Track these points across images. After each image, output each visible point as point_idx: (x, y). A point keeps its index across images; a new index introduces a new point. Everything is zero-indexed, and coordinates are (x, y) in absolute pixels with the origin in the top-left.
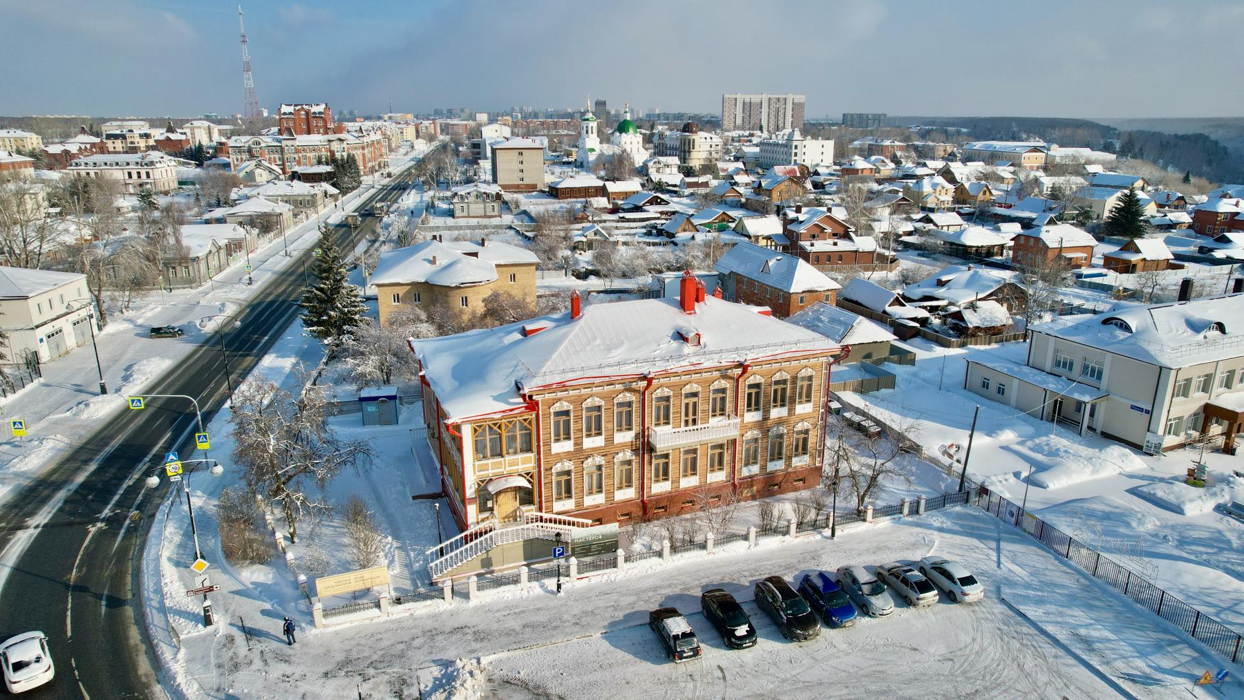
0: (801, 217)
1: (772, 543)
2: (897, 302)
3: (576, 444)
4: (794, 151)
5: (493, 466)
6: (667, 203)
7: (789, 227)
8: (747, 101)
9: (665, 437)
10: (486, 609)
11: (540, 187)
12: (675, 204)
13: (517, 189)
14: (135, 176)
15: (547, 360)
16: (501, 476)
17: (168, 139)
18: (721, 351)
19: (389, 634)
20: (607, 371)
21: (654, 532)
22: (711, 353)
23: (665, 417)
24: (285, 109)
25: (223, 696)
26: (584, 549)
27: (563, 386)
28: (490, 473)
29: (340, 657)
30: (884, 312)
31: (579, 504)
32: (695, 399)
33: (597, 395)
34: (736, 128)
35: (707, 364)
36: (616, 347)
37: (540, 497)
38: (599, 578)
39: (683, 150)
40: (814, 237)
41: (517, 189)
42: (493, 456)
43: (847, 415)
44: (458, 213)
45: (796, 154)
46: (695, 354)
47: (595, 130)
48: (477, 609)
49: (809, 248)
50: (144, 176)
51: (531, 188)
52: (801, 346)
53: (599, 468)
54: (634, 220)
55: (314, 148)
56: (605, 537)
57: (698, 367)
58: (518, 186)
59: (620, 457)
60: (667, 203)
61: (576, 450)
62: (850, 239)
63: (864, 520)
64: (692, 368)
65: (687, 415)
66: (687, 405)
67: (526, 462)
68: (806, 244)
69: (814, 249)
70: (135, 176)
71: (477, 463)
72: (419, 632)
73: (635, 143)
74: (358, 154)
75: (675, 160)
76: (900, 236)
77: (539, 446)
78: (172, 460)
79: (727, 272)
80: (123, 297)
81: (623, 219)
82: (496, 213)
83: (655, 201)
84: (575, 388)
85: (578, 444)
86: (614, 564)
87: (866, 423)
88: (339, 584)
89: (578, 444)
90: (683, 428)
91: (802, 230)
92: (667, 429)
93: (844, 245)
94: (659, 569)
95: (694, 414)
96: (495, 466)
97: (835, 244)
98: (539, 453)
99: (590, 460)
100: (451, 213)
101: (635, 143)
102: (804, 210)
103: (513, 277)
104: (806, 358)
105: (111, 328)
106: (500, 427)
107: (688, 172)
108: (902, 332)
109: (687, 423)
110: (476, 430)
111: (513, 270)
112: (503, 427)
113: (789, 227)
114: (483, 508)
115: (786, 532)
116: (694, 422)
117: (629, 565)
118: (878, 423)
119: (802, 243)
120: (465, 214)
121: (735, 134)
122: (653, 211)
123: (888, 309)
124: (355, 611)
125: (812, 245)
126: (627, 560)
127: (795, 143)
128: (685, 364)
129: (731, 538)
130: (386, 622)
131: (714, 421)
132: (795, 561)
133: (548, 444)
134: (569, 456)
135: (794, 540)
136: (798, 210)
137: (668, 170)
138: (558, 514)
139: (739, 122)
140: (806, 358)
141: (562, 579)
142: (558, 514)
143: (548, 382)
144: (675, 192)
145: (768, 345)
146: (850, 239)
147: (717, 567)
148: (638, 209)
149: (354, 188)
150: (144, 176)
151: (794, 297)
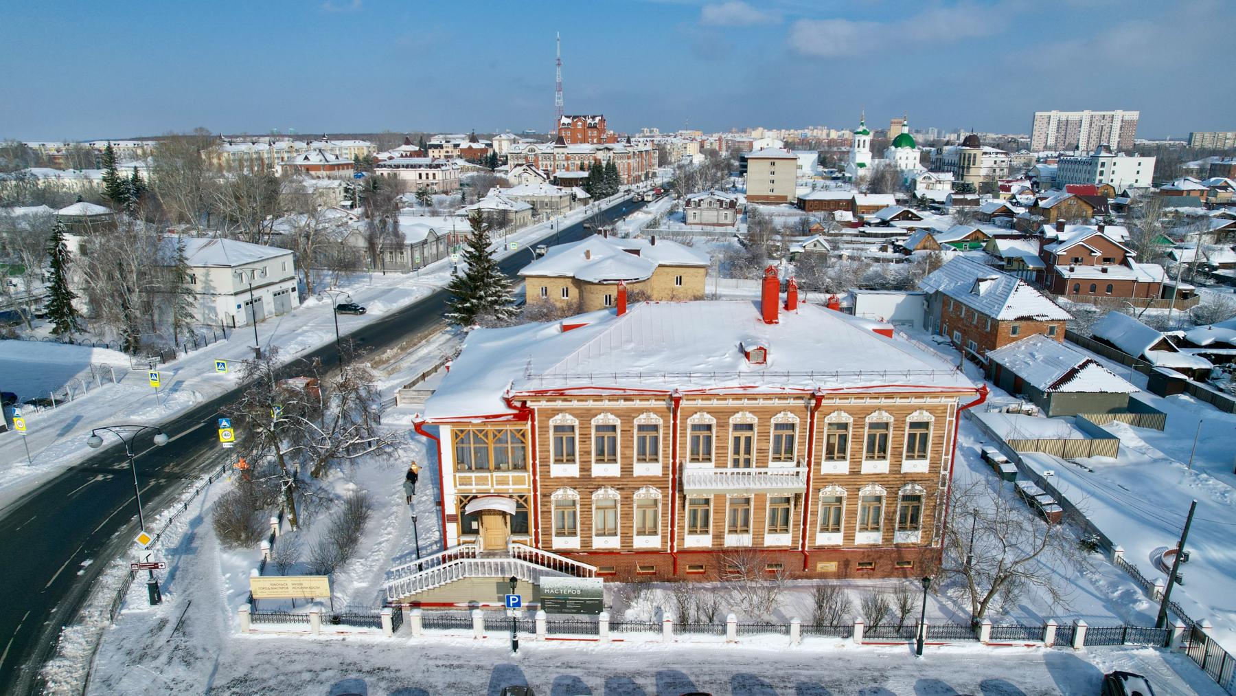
0: (1062, 236)
1: (824, 646)
2: (1164, 345)
3: (582, 470)
4: (1100, 169)
5: (476, 482)
6: (920, 219)
7: (1046, 247)
8: (1064, 118)
9: (700, 477)
10: (424, 652)
11: (790, 199)
12: (930, 219)
13: (767, 200)
14: (424, 177)
15: (558, 361)
16: (488, 495)
17: (470, 148)
18: (788, 375)
19: (307, 657)
20: (623, 383)
21: (655, 601)
22: (775, 374)
23: (702, 453)
24: (565, 120)
25: (197, 678)
26: (557, 603)
27: (560, 394)
28: (474, 488)
29: (240, 672)
30: (1143, 357)
31: (586, 543)
32: (748, 434)
33: (612, 411)
34: (1046, 148)
35: (764, 388)
36: (650, 354)
37: (536, 527)
38: (574, 645)
39: (960, 167)
40: (1076, 260)
41: (767, 200)
42: (515, 468)
43: (1024, 485)
44: (690, 219)
45: (1101, 173)
46: (752, 374)
47: (868, 144)
48: (413, 649)
49: (1066, 274)
50: (431, 177)
51: (779, 200)
52: (912, 380)
53: (839, 500)
54: (876, 235)
55: (582, 156)
56: (584, 592)
57: (750, 391)
58: (767, 197)
59: (867, 491)
60: (920, 219)
61: (582, 477)
62: (1128, 265)
63: (978, 639)
64: (741, 391)
65: (737, 451)
66: (737, 440)
67: (519, 482)
68: (1064, 270)
69: (1073, 276)
70: (424, 177)
71: (458, 475)
72: (335, 662)
73: (911, 158)
74: (621, 164)
75: (949, 177)
76: (1216, 268)
77: (534, 465)
78: (225, 427)
79: (932, 292)
80: (328, 276)
81: (864, 234)
82: (727, 222)
83: (905, 216)
84: (582, 398)
85: (585, 468)
86: (595, 629)
87: (1046, 500)
88: (274, 586)
89: (585, 468)
90: (730, 469)
91: (1060, 251)
92: (708, 468)
93: (1116, 273)
94: (654, 648)
95: (748, 451)
96: (480, 481)
97: (1104, 271)
98: (534, 474)
99: (601, 492)
100: (684, 220)
101: (911, 158)
102: (1067, 227)
103: (679, 281)
104: (919, 395)
105: (311, 301)
106: (486, 436)
107: (964, 188)
108: (1160, 384)
109: (736, 463)
110: (457, 436)
111: (680, 271)
112: (491, 436)
113: (1046, 247)
114: (466, 530)
115: (849, 632)
116: (748, 463)
117: (616, 635)
118: (1062, 501)
119: (1059, 268)
120: (697, 221)
121: (1042, 155)
122: (900, 226)
123: (1149, 354)
124: (285, 621)
125: (1072, 270)
126: (614, 626)
127: (1101, 160)
128: (734, 384)
129: (766, 627)
130: (314, 642)
131: (774, 467)
132: (845, 677)
133: (818, 464)
134: (572, 483)
135: (855, 647)
136: (1060, 227)
137: (939, 186)
138: (556, 552)
139: (1051, 142)
140: (889, 396)
141: (521, 635)
142: (556, 552)
143: (543, 388)
144: (938, 209)
145: (860, 374)
146: (1128, 265)
147: (733, 663)
148: (885, 223)
149: (607, 195)
150: (431, 177)
151: (1002, 326)
